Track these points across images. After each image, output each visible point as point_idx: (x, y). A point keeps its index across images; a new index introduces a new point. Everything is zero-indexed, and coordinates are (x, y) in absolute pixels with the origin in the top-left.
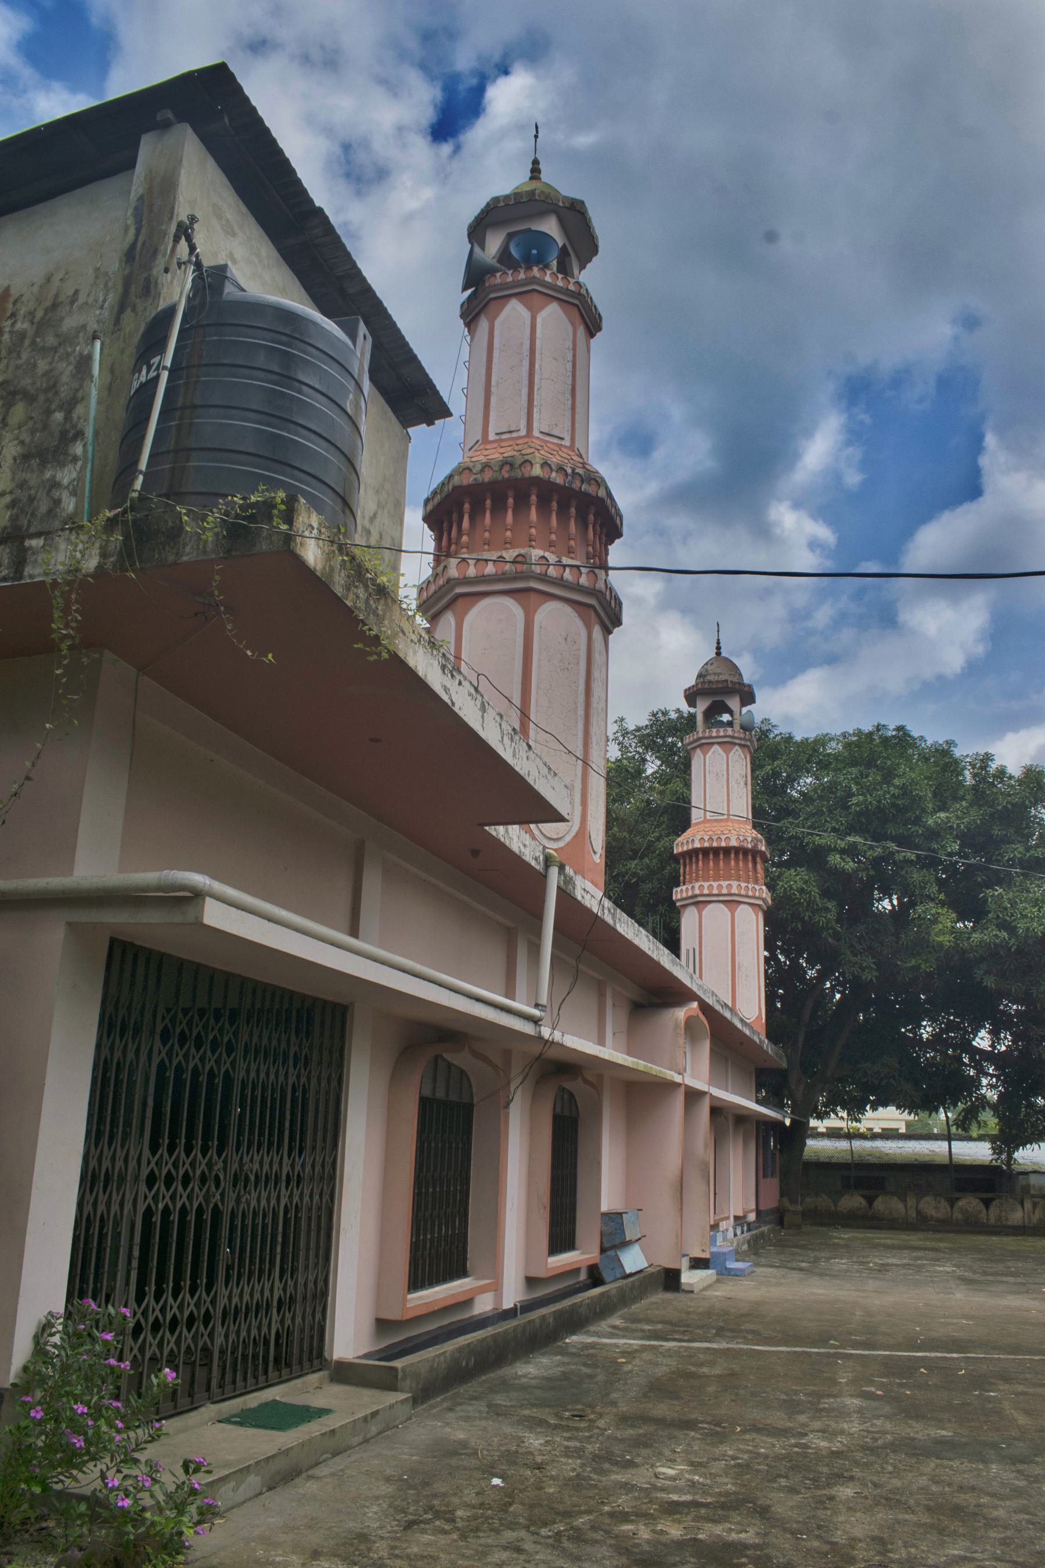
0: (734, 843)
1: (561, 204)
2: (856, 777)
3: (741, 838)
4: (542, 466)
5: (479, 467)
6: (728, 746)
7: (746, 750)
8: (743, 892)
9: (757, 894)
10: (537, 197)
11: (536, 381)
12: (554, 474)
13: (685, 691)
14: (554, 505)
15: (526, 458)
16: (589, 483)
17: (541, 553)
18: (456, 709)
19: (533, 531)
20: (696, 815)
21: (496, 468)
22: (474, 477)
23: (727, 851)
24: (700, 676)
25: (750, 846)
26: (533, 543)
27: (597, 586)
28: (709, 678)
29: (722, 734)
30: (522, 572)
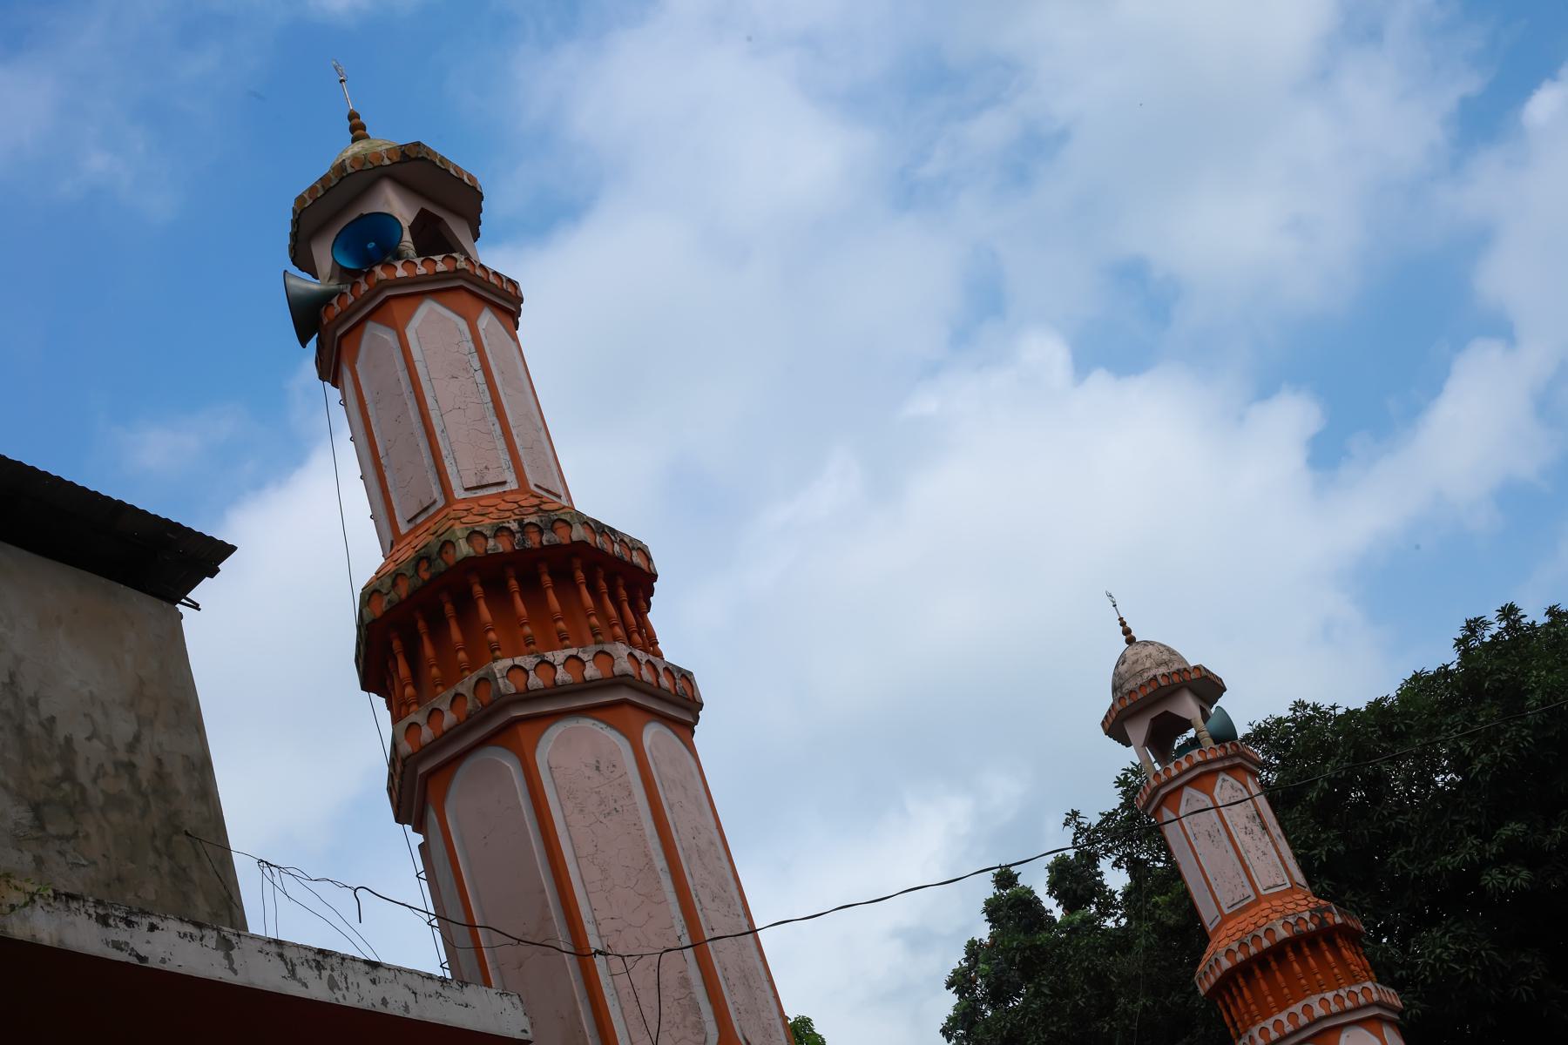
0: (1282, 933)
1: (387, 162)
2: (1465, 728)
3: (1291, 920)
4: (468, 539)
5: (389, 582)
6: (1206, 781)
7: (1240, 773)
8: (1334, 1008)
9: (1362, 1000)
10: (350, 170)
11: (435, 421)
12: (491, 542)
13: (1103, 724)
14: (514, 584)
15: (443, 538)
16: (553, 530)
17: (508, 662)
18: (153, 963)
19: (492, 636)
20: (1208, 914)
21: (410, 573)
22: (386, 598)
23: (1278, 951)
24: (1115, 689)
25: (1312, 926)
26: (498, 653)
27: (617, 670)
28: (1128, 686)
29: (1185, 765)
30: (492, 703)
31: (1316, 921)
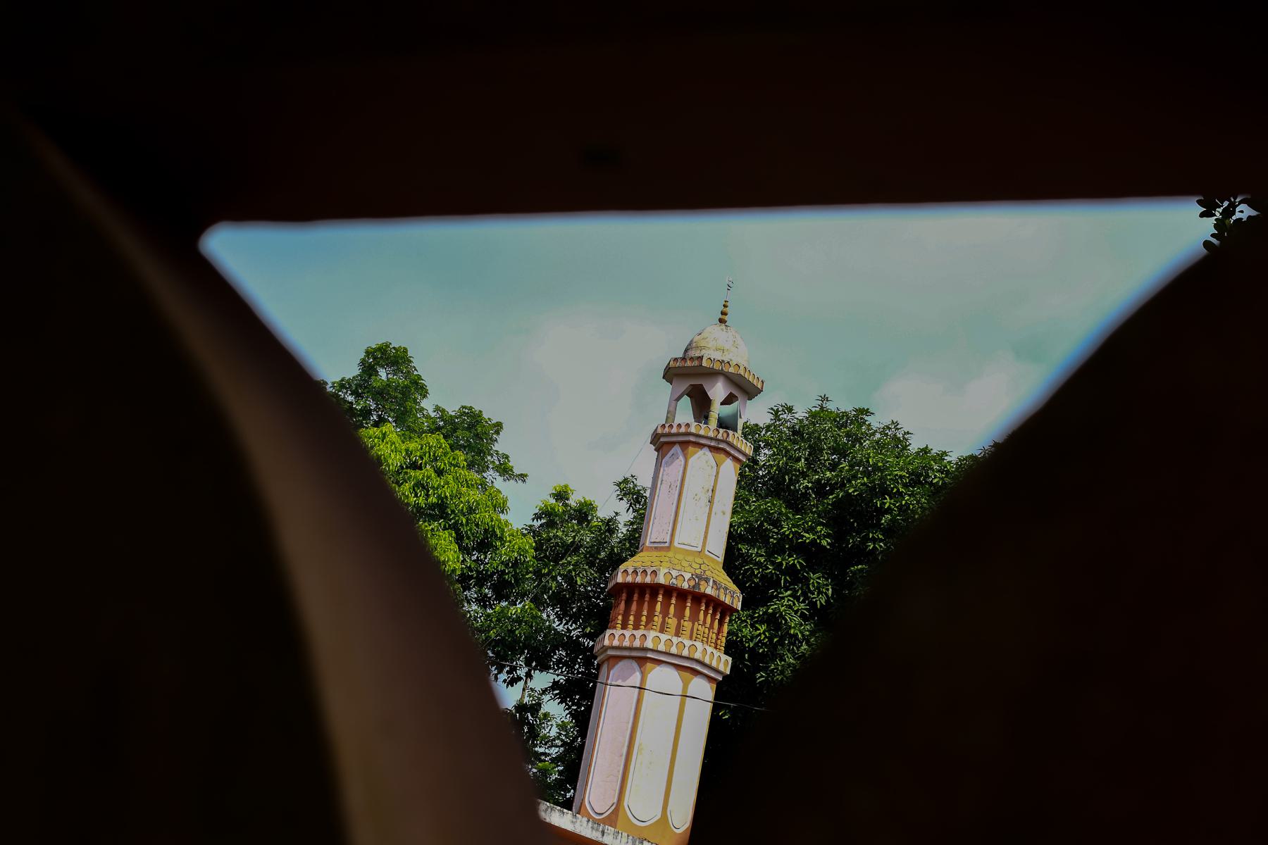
0: (661, 579)
3: (675, 573)
31: (692, 583)
